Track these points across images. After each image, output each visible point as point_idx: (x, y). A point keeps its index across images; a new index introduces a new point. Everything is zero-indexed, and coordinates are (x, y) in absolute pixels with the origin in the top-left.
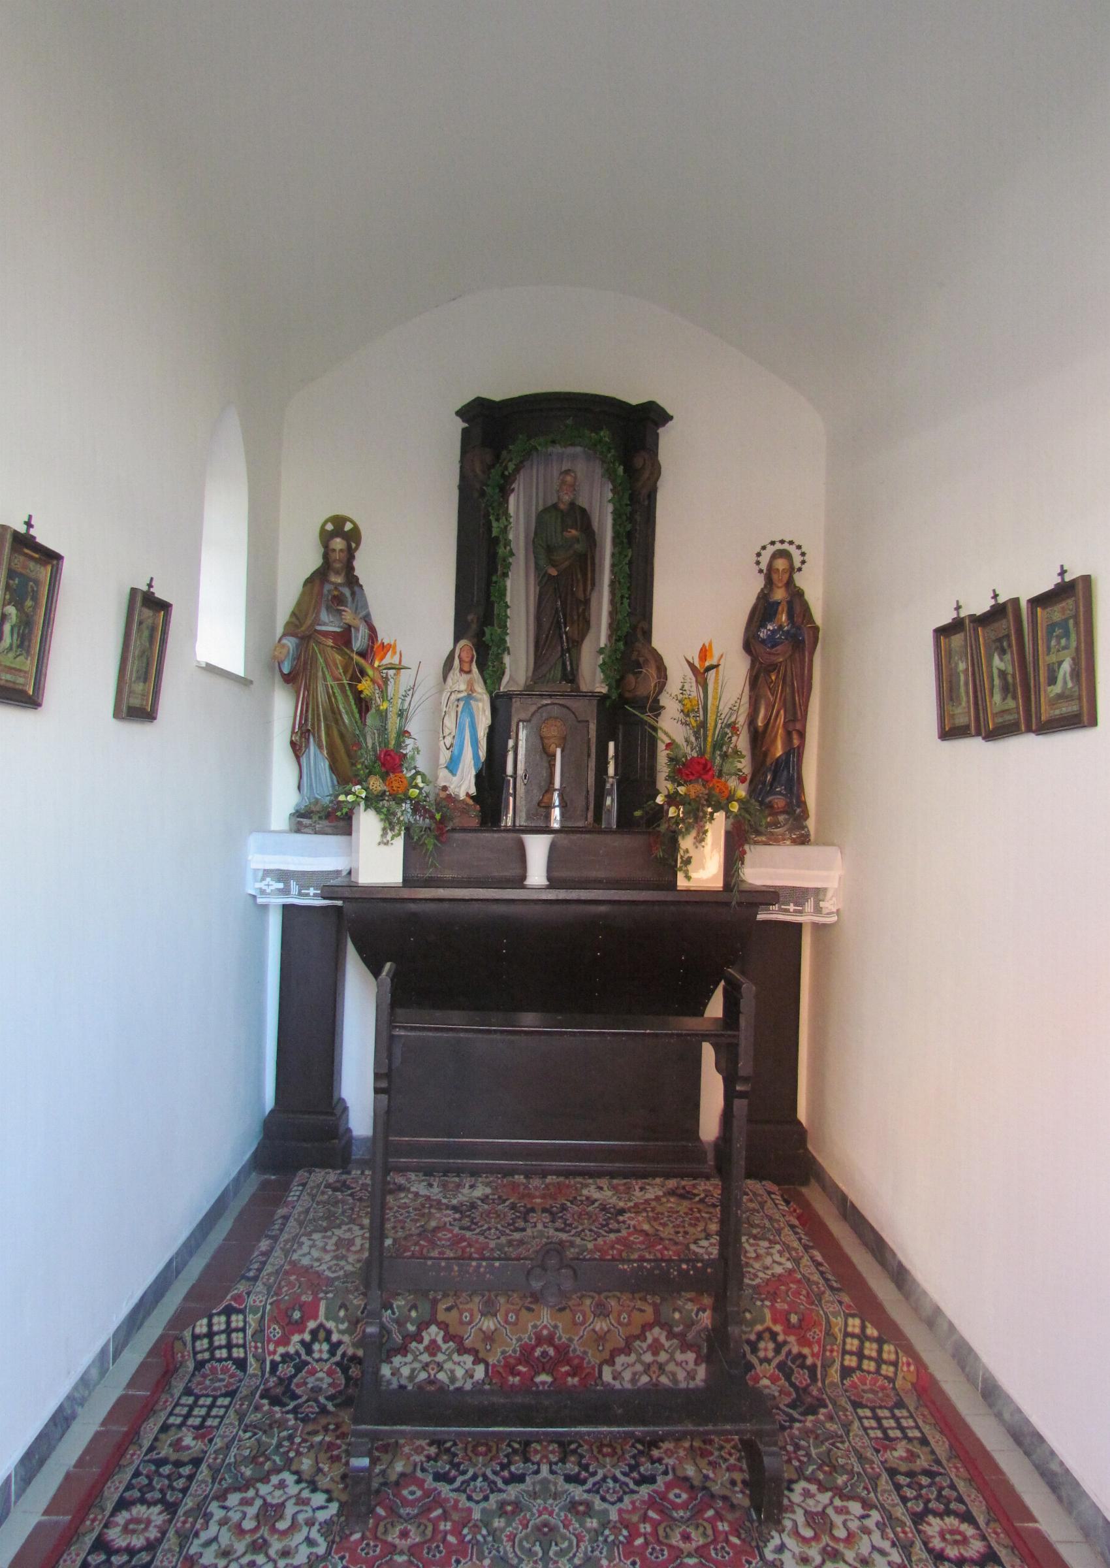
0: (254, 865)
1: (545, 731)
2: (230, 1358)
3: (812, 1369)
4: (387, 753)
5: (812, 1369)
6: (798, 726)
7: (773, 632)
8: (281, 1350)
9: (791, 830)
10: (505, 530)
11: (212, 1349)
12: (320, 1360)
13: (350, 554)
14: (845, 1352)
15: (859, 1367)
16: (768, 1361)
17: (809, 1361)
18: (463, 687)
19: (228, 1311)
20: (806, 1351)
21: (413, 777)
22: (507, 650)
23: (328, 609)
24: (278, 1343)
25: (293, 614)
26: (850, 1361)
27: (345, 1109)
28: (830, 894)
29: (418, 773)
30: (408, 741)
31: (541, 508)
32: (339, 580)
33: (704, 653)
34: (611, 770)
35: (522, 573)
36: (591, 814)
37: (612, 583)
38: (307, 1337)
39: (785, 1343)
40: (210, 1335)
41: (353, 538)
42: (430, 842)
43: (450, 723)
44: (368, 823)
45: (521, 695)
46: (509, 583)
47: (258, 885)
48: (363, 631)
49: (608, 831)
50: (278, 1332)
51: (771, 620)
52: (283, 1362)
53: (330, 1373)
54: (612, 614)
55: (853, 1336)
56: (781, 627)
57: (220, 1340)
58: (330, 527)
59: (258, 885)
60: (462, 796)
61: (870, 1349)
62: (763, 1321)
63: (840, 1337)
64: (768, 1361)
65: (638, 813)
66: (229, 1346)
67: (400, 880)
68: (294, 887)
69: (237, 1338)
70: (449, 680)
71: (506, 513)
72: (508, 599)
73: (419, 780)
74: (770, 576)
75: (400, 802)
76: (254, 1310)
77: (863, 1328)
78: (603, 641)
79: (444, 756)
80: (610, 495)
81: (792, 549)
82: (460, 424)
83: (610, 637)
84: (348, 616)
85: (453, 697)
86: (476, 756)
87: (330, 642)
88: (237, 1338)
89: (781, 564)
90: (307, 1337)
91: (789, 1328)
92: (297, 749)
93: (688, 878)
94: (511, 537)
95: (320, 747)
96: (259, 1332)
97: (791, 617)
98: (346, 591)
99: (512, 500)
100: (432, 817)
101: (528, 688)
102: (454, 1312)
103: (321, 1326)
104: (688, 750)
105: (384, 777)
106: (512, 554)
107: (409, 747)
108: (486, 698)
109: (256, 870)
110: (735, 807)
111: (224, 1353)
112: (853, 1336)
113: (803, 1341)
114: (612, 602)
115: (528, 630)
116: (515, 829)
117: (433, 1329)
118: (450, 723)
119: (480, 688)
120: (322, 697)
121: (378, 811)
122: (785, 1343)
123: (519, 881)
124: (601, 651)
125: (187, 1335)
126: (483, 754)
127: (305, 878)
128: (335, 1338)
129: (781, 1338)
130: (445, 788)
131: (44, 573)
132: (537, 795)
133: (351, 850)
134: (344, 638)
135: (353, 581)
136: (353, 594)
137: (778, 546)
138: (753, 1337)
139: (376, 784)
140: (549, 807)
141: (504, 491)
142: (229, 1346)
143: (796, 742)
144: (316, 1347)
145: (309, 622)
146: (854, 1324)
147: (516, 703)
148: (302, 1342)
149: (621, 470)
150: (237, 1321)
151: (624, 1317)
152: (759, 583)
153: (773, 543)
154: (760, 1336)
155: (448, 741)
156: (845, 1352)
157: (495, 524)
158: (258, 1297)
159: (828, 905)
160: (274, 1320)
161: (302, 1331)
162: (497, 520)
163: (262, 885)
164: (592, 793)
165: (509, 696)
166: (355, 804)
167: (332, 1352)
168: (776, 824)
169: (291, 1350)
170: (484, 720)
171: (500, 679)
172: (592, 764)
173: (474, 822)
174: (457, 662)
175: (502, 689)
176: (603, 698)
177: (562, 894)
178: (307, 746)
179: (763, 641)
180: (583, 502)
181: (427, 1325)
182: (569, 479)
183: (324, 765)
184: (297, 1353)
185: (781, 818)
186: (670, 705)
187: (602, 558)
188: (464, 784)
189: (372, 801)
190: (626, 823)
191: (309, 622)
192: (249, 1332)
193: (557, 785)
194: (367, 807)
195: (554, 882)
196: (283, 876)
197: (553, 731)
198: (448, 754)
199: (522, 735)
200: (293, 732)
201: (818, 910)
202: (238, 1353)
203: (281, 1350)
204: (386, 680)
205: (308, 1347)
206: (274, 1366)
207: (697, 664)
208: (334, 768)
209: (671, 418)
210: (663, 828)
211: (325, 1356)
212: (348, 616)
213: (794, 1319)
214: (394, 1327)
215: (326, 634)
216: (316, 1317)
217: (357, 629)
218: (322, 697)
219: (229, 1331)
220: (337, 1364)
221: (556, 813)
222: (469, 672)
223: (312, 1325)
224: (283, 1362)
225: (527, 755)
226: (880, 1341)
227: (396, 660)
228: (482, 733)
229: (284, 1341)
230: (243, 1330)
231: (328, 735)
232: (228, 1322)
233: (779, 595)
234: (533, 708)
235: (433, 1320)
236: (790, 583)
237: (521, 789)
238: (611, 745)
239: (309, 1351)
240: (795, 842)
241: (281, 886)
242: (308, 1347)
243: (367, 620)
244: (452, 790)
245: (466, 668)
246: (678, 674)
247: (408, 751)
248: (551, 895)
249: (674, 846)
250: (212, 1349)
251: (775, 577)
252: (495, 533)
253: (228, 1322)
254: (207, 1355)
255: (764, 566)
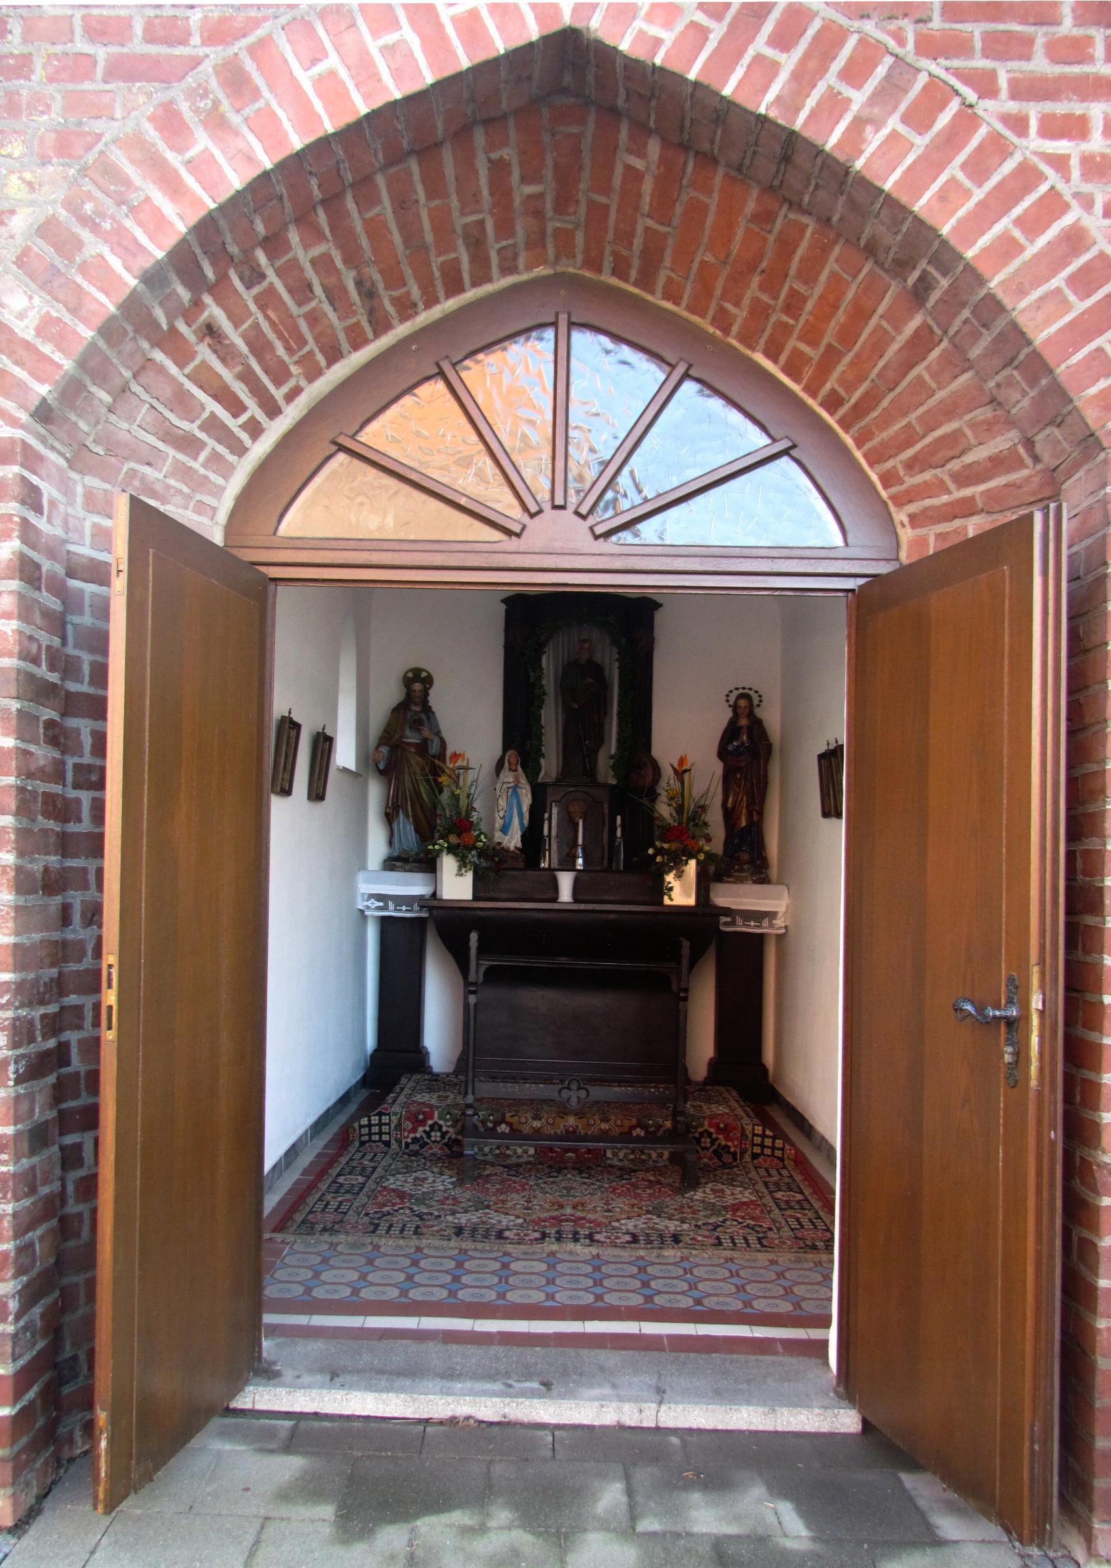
0: (362, 891)
1: (571, 809)
2: (380, 1140)
3: (735, 1153)
4: (461, 821)
5: (734, 1154)
6: (757, 808)
7: (738, 747)
8: (412, 1135)
9: (752, 875)
10: (539, 678)
11: (370, 1134)
12: (435, 1141)
13: (426, 694)
14: (754, 1145)
15: (762, 1153)
16: (707, 1149)
17: (732, 1150)
18: (511, 780)
19: (380, 1114)
20: (730, 1144)
21: (479, 836)
22: (543, 755)
23: (411, 728)
24: (410, 1132)
25: (385, 731)
26: (757, 1150)
27: (428, 1053)
28: (780, 915)
29: (481, 833)
30: (474, 813)
31: (566, 662)
32: (418, 709)
33: (682, 761)
34: (619, 833)
35: (553, 705)
36: (605, 862)
37: (619, 714)
38: (427, 1129)
39: (717, 1139)
40: (370, 1126)
41: (428, 681)
42: (492, 875)
43: (502, 803)
44: (448, 864)
45: (554, 785)
46: (543, 712)
47: (366, 903)
48: (436, 741)
49: (619, 871)
50: (410, 1126)
51: (736, 739)
52: (413, 1143)
53: (441, 1149)
54: (619, 733)
55: (758, 1135)
56: (743, 744)
57: (375, 1129)
58: (410, 675)
59: (366, 903)
60: (512, 848)
61: (768, 1142)
62: (703, 1126)
63: (750, 1136)
64: (707, 1149)
65: (635, 859)
66: (380, 1133)
67: (469, 896)
68: (391, 905)
69: (385, 1129)
70: (502, 775)
71: (541, 669)
72: (543, 723)
73: (482, 837)
74: (735, 708)
75: (470, 850)
76: (395, 1114)
77: (764, 1131)
78: (613, 751)
79: (499, 823)
80: (617, 656)
81: (752, 693)
82: (504, 607)
83: (618, 748)
84: (426, 733)
85: (505, 786)
86: (521, 823)
87: (413, 750)
88: (385, 1129)
89: (742, 703)
90: (427, 1129)
91: (719, 1130)
92: (389, 817)
93: (671, 900)
94: (544, 682)
95: (407, 816)
96: (399, 1126)
97: (750, 736)
98: (424, 717)
99: (544, 659)
100: (493, 860)
101: (558, 780)
102: (516, 1118)
103: (436, 1123)
104: (671, 821)
105: (459, 835)
106: (545, 694)
107: (474, 817)
108: (528, 787)
109: (363, 894)
110: (702, 857)
111: (377, 1138)
112: (758, 1135)
113: (727, 1138)
114: (619, 725)
115: (557, 720)
116: (550, 870)
117: (503, 1126)
118: (502, 803)
119: (523, 781)
120: (408, 785)
121: (456, 855)
122: (717, 1139)
123: (555, 899)
124: (612, 757)
125: (356, 1125)
126: (526, 822)
127: (399, 900)
128: (444, 1129)
129: (714, 1136)
130: (499, 843)
131: (293, 733)
132: (566, 850)
133: (436, 882)
134: (422, 748)
135: (427, 710)
136: (428, 718)
137: (741, 691)
138: (697, 1135)
139: (453, 839)
140: (575, 857)
141: (539, 653)
142: (380, 1133)
143: (755, 818)
144: (433, 1134)
145: (397, 736)
146: (759, 1130)
147: (550, 790)
148: (425, 1131)
149: (624, 640)
150: (385, 1119)
151: (619, 1122)
152: (729, 713)
153: (737, 689)
154: (701, 1134)
155: (502, 813)
156: (754, 1145)
157: (532, 674)
158: (396, 1108)
159: (779, 922)
160: (408, 1119)
161: (424, 1125)
162: (534, 671)
163: (368, 903)
164: (606, 847)
165: (544, 786)
166: (441, 851)
167: (443, 1137)
168: (741, 871)
169: (418, 1135)
170: (527, 801)
171: (538, 774)
172: (606, 830)
173: (521, 865)
174: (506, 764)
175: (539, 780)
176: (612, 788)
177: (583, 907)
178: (398, 815)
179: (731, 752)
180: (598, 658)
181: (500, 1124)
182: (586, 645)
183: (410, 828)
184: (422, 1138)
185: (745, 867)
186: (662, 789)
187: (612, 698)
188: (513, 840)
189: (452, 850)
190: (629, 867)
191: (397, 736)
192: (393, 1126)
193: (580, 841)
194: (448, 853)
195: (576, 897)
196: (379, 897)
197: (576, 808)
198: (501, 822)
199: (555, 811)
200: (387, 806)
201: (771, 926)
202: (385, 1138)
203: (412, 1135)
204: (458, 777)
205: (428, 1134)
206: (407, 1145)
207: (676, 766)
208: (417, 831)
209: (661, 605)
210: (653, 868)
211: (438, 1139)
212: (426, 733)
213: (722, 1126)
214: (480, 1125)
215: (409, 744)
216: (432, 1118)
217: (432, 741)
218: (408, 785)
219: (380, 1124)
220: (445, 1144)
221: (580, 861)
222: (515, 770)
223: (430, 1122)
224: (413, 1143)
225: (559, 821)
226: (774, 1138)
227: (465, 764)
228: (525, 809)
229: (414, 1130)
230: (389, 1124)
231: (413, 808)
232: (380, 1120)
233: (743, 722)
234: (562, 793)
235: (503, 1121)
236: (751, 715)
237: (554, 847)
238: (619, 818)
239: (429, 1137)
240: (755, 882)
241: (381, 904)
242: (428, 1134)
243: (438, 733)
244: (505, 844)
245: (513, 767)
246: (668, 773)
247: (474, 819)
248: (576, 907)
249: (663, 880)
250: (370, 1134)
251: (739, 711)
252: (532, 680)
253: (380, 1120)
254: (367, 1138)
255: (731, 702)
